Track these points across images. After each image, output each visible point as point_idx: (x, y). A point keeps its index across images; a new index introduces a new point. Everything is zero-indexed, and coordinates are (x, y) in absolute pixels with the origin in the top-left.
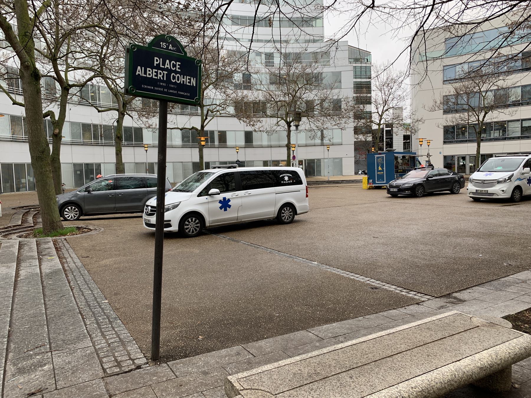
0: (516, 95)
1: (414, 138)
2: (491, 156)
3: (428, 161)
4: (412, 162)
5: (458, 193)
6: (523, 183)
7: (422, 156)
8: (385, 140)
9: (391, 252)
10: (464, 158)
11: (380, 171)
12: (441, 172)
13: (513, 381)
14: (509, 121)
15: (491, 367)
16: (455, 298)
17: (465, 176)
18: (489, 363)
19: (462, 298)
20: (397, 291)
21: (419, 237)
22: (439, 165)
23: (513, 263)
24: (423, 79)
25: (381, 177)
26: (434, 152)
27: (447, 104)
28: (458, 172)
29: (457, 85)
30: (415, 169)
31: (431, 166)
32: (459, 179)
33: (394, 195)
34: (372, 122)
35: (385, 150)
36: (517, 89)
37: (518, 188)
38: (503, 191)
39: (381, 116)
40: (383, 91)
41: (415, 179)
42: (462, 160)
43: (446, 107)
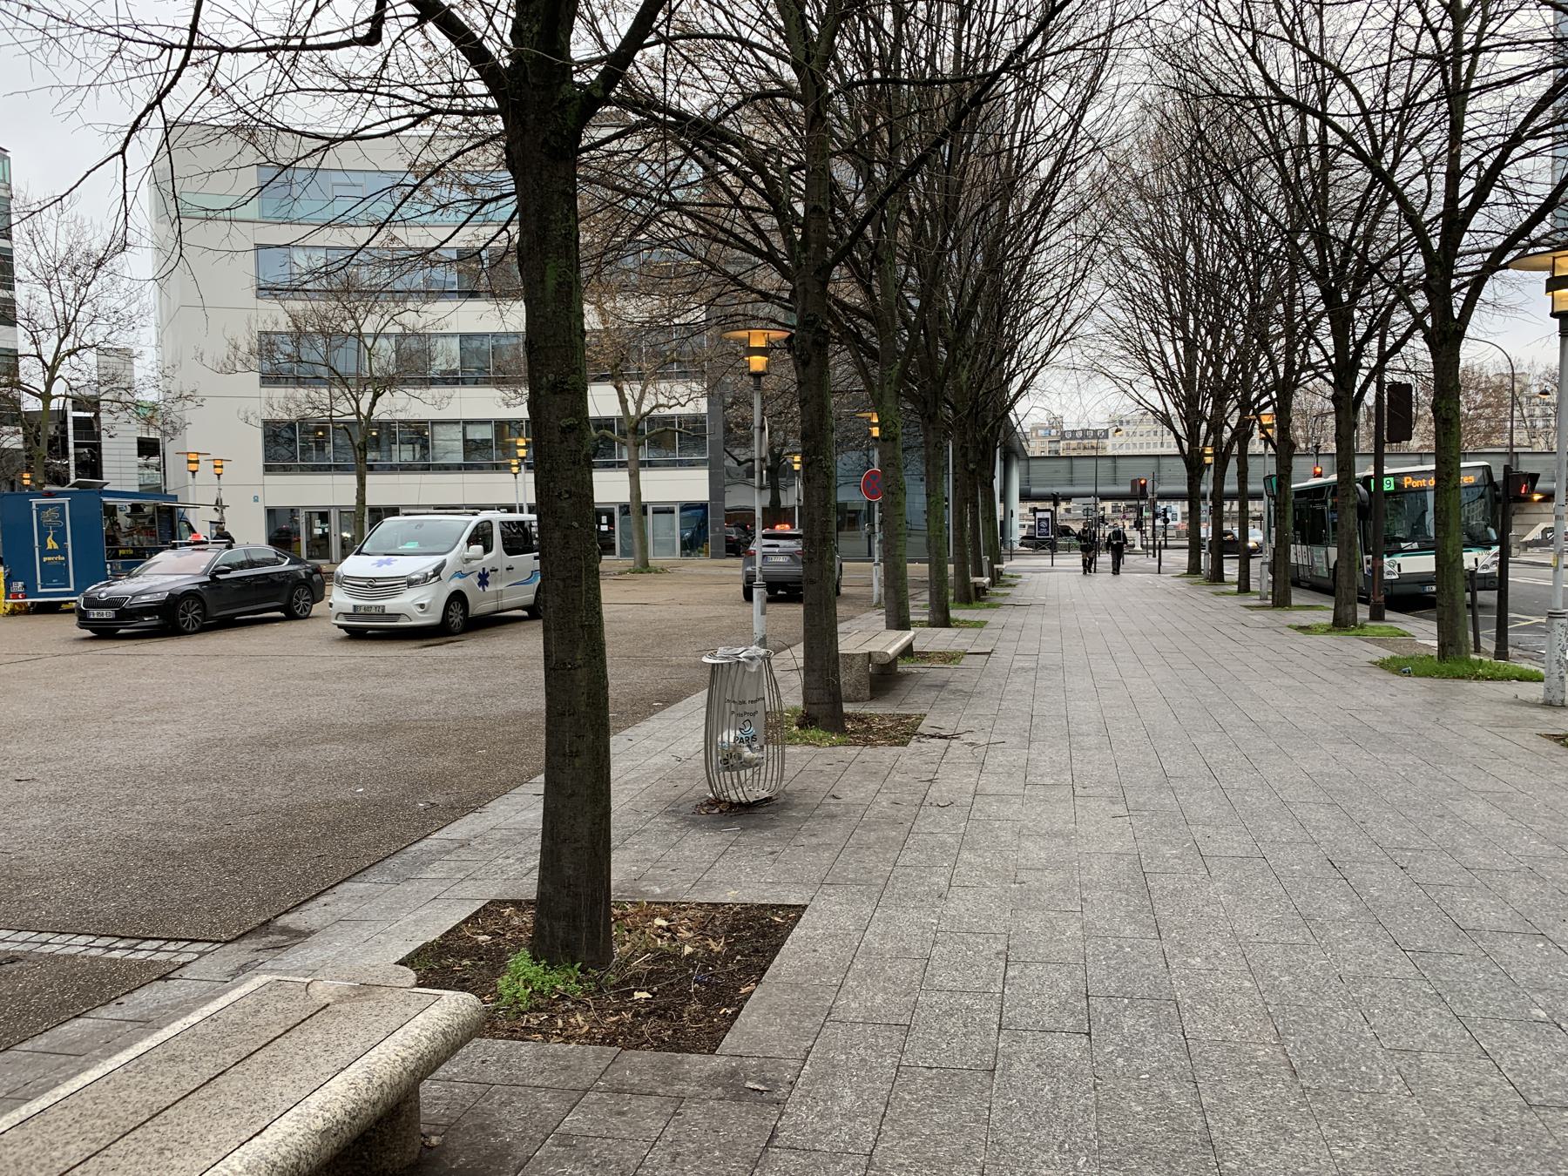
0: (447, 356)
1: (170, 448)
2: (394, 511)
3: (218, 525)
4: (162, 524)
5: (307, 617)
6: (469, 585)
7: (196, 506)
8: (71, 451)
9: (82, 822)
10: (324, 517)
11: (53, 553)
12: (255, 557)
13: (424, 1129)
14: (434, 423)
15: (354, 1118)
16: (285, 930)
17: (325, 568)
18: (348, 1107)
19: (302, 926)
20: (93, 952)
21: (179, 762)
22: (252, 537)
23: (440, 799)
24: (171, 265)
25: (55, 574)
26: (235, 497)
27: (271, 357)
28: (310, 557)
29: (298, 306)
30: (174, 547)
31: (223, 536)
32: (310, 576)
33: (103, 633)
34: (18, 385)
35: (73, 480)
36: (449, 339)
37: (458, 598)
38: (422, 606)
39: (51, 370)
40: (55, 289)
41: (173, 578)
42: (317, 522)
43: (267, 366)
